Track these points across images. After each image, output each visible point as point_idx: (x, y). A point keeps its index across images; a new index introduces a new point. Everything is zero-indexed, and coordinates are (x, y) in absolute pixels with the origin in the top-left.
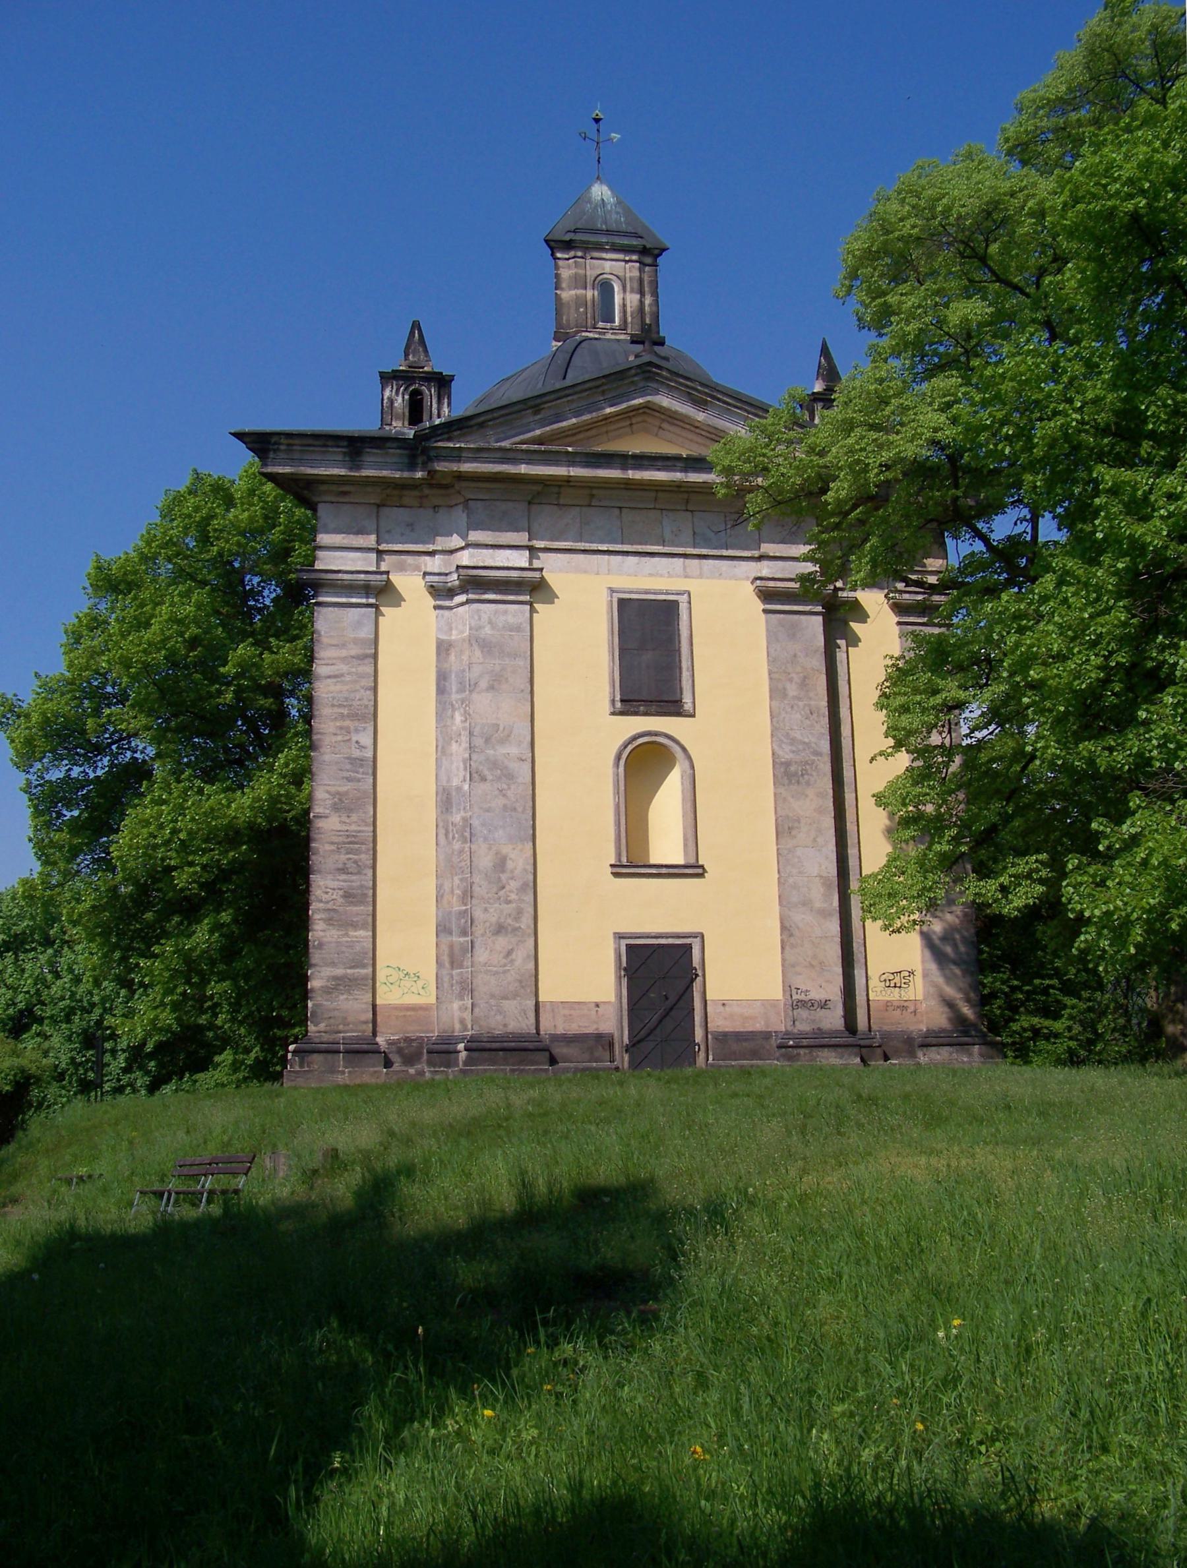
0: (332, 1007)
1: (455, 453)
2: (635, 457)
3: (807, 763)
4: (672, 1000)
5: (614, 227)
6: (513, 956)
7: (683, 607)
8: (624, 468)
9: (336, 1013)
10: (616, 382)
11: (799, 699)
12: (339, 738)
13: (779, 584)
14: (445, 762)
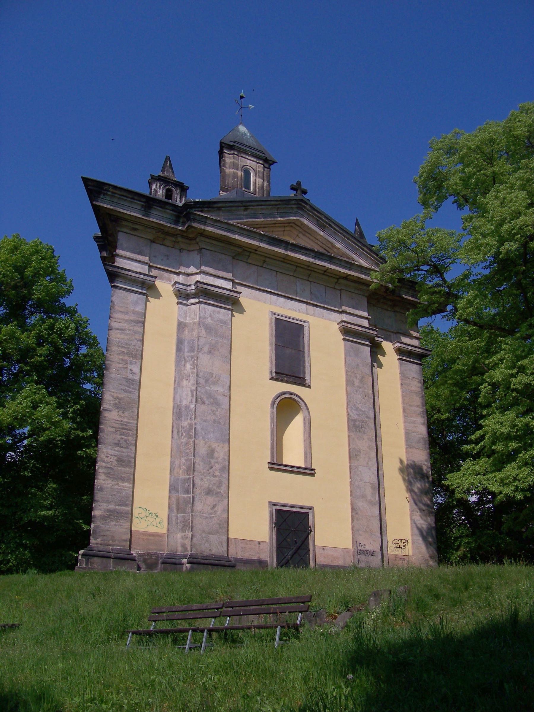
0: (105, 531)
1: (204, 220)
2: (292, 244)
3: (363, 422)
4: (299, 544)
6: (216, 508)
7: (306, 329)
9: (108, 533)
11: (360, 388)
12: (121, 365)
13: (353, 327)
14: (179, 391)
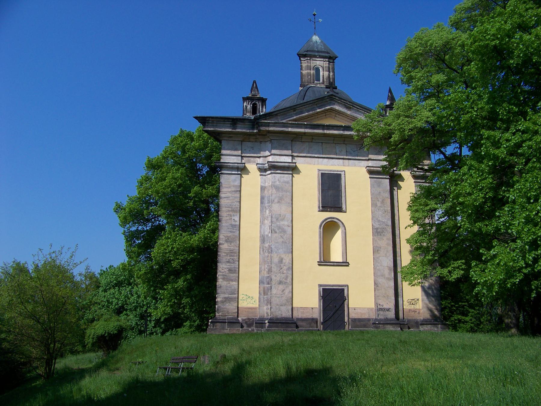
0: (224, 307)
2: (327, 126)
4: (337, 307)
5: (320, 50)
7: (343, 176)
8: (323, 129)
10: (321, 101)
12: (228, 218)
13: (375, 169)
